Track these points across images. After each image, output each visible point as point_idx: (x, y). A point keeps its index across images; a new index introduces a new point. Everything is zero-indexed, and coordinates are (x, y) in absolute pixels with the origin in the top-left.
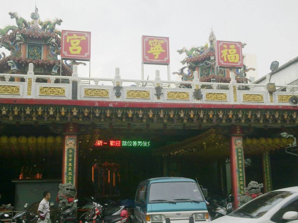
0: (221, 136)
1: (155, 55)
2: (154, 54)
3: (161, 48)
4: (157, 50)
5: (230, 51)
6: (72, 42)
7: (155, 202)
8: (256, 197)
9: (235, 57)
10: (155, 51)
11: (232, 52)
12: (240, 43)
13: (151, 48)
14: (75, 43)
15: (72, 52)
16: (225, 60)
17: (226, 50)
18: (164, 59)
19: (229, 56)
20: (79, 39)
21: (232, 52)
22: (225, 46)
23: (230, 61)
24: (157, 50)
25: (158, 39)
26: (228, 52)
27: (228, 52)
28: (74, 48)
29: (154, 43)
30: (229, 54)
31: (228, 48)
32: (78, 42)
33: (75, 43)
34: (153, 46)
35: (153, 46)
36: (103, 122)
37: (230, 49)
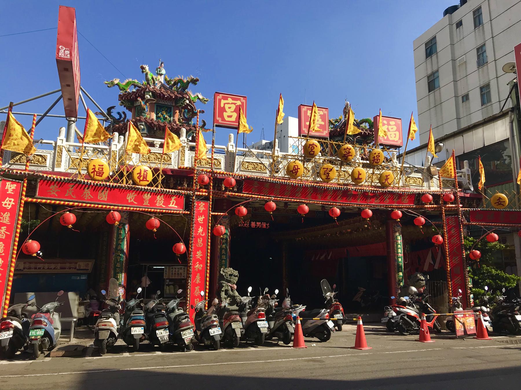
3: (320, 120)
5: (390, 127)
6: (227, 106)
9: (395, 134)
11: (392, 129)
14: (230, 108)
15: (227, 119)
20: (235, 104)
21: (392, 129)
23: (391, 139)
28: (230, 114)
30: (389, 131)
32: (233, 107)
33: (230, 108)
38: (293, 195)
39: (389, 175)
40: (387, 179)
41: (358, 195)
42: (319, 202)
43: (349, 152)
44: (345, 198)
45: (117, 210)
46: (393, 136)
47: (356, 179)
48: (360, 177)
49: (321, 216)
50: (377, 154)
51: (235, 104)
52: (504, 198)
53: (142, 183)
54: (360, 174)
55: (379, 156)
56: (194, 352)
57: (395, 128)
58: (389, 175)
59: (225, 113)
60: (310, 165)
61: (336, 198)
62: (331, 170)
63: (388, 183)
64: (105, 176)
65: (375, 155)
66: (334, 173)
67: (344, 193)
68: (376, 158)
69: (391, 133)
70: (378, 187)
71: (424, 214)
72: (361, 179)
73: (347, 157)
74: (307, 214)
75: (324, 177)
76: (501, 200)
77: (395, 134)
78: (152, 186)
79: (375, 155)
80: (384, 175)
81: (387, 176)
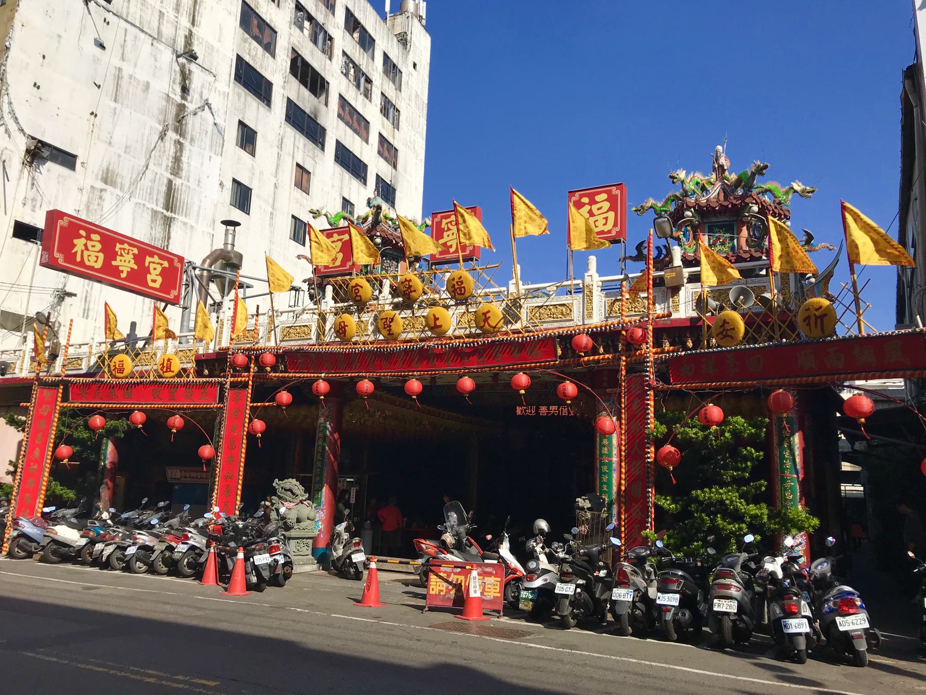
0: (344, 524)
1: (122, 272)
2: (121, 268)
3: (132, 261)
4: (126, 264)
5: (90, 243)
6: (152, 266)
7: (860, 332)
8: (865, 222)
9: (97, 257)
10: (122, 263)
11: (93, 246)
12: (181, 259)
13: (118, 258)
14: (155, 269)
15: (151, 284)
16: (78, 259)
17: (83, 241)
18: (169, 294)
19: (86, 253)
20: (161, 264)
21: (93, 246)
22: (82, 233)
23: (87, 263)
24: (126, 264)
25: (130, 245)
26: (86, 245)
27: (86, 245)
28: (155, 278)
29: (124, 249)
30: (87, 249)
31: (88, 238)
32: (159, 268)
33: (155, 269)
34: (121, 255)
35: (121, 255)
36: (216, 449)
37: (91, 240)
38: (349, 368)
39: (489, 312)
40: (486, 320)
41: (445, 354)
42: (487, 369)
43: (410, 287)
44: (425, 362)
45: (139, 410)
46: (93, 259)
47: (435, 326)
48: (438, 323)
49: (439, 395)
50: (456, 280)
51: (161, 264)
52: (733, 321)
53: (166, 375)
54: (436, 319)
55: (462, 282)
56: (504, 619)
57: (99, 246)
58: (489, 312)
59: (148, 276)
60: (367, 317)
61: (411, 363)
62: (392, 319)
63: (489, 325)
64: (126, 372)
65: (455, 282)
66: (397, 324)
67: (418, 356)
68: (456, 286)
69: (89, 253)
70: (478, 336)
71: (576, 378)
72: (440, 326)
73: (409, 295)
74: (470, 393)
75: (385, 332)
76: (727, 327)
77: (97, 257)
78: (182, 377)
79: (455, 282)
80: (480, 313)
81: (484, 314)
